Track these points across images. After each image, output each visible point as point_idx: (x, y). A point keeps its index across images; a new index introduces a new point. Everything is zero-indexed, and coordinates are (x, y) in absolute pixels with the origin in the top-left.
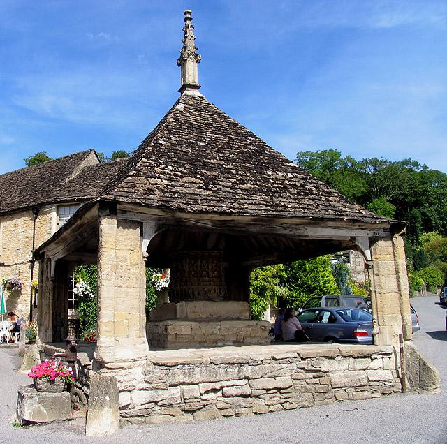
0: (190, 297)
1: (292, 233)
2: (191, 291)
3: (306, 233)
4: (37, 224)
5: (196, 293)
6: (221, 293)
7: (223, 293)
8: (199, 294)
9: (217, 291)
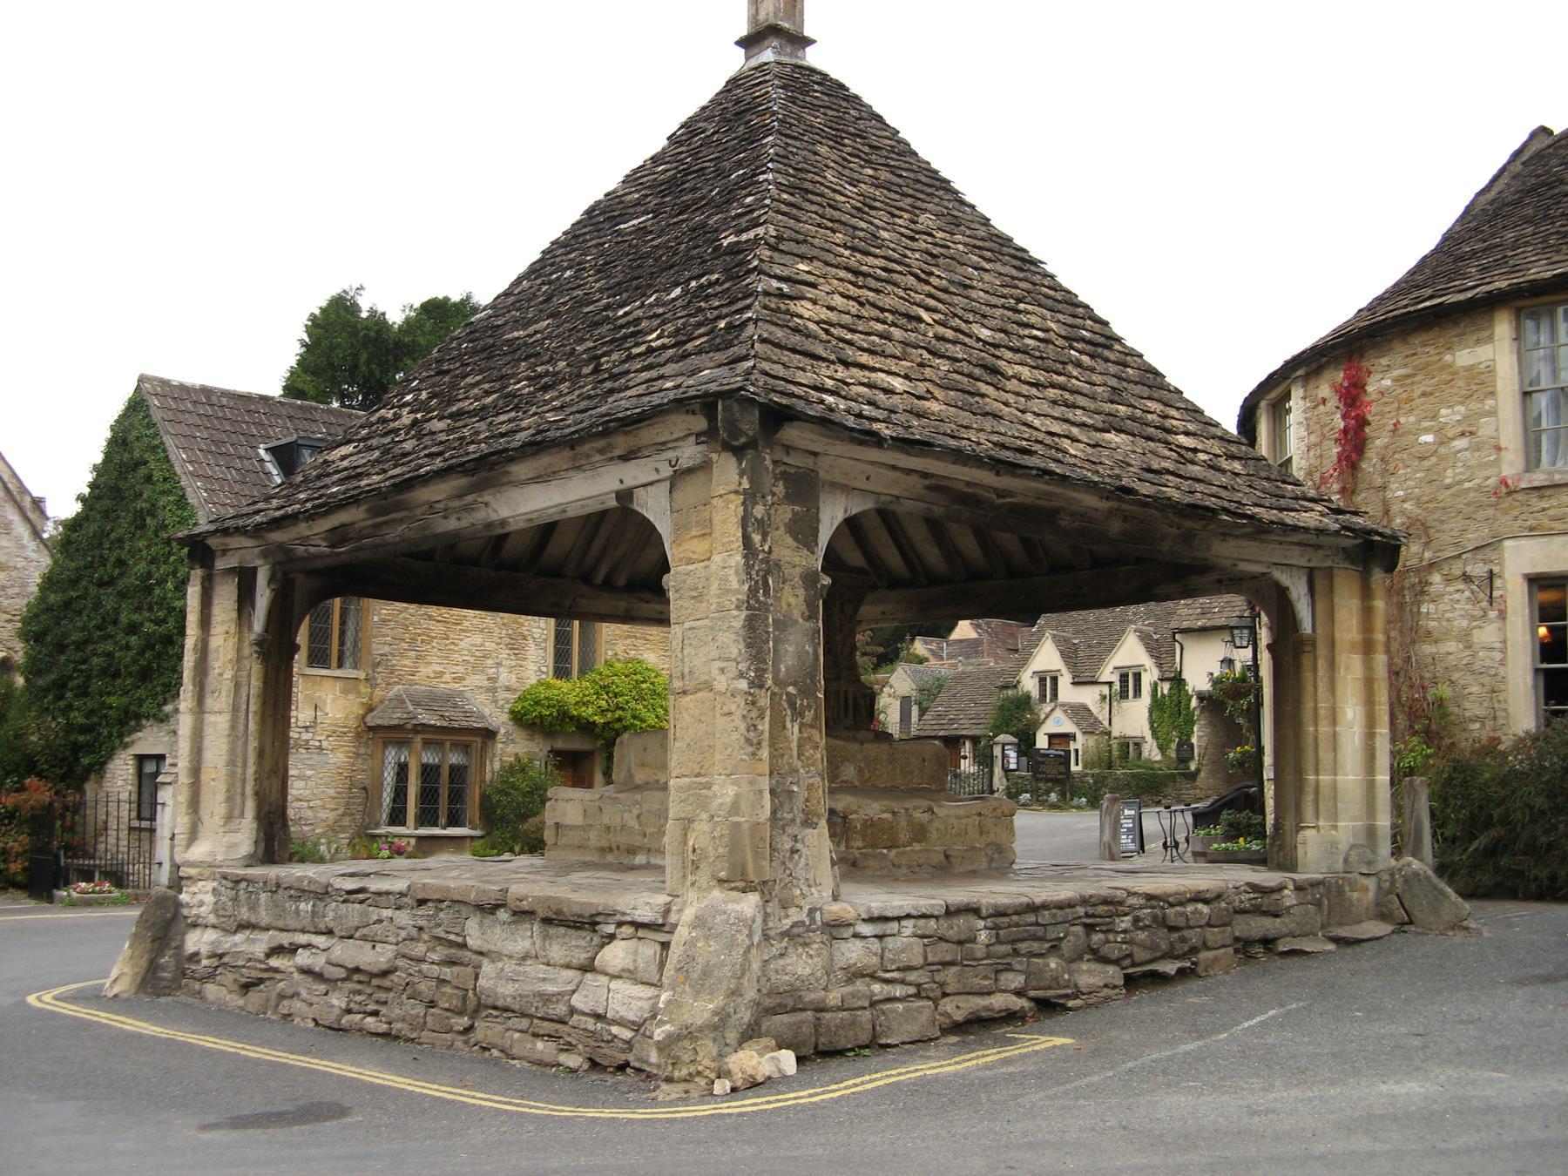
1: (464, 523)
3: (494, 517)
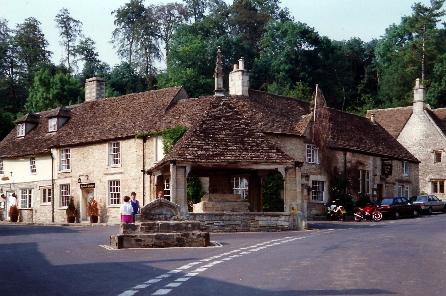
4: (146, 147)
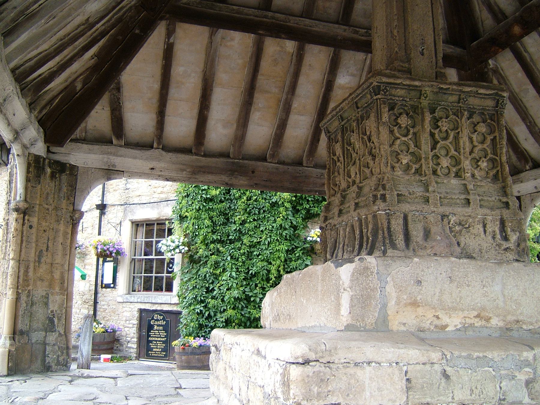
0: (394, 246)
2: (397, 225)
5: (417, 233)
6: (506, 238)
7: (514, 237)
8: (427, 234)
9: (494, 227)
